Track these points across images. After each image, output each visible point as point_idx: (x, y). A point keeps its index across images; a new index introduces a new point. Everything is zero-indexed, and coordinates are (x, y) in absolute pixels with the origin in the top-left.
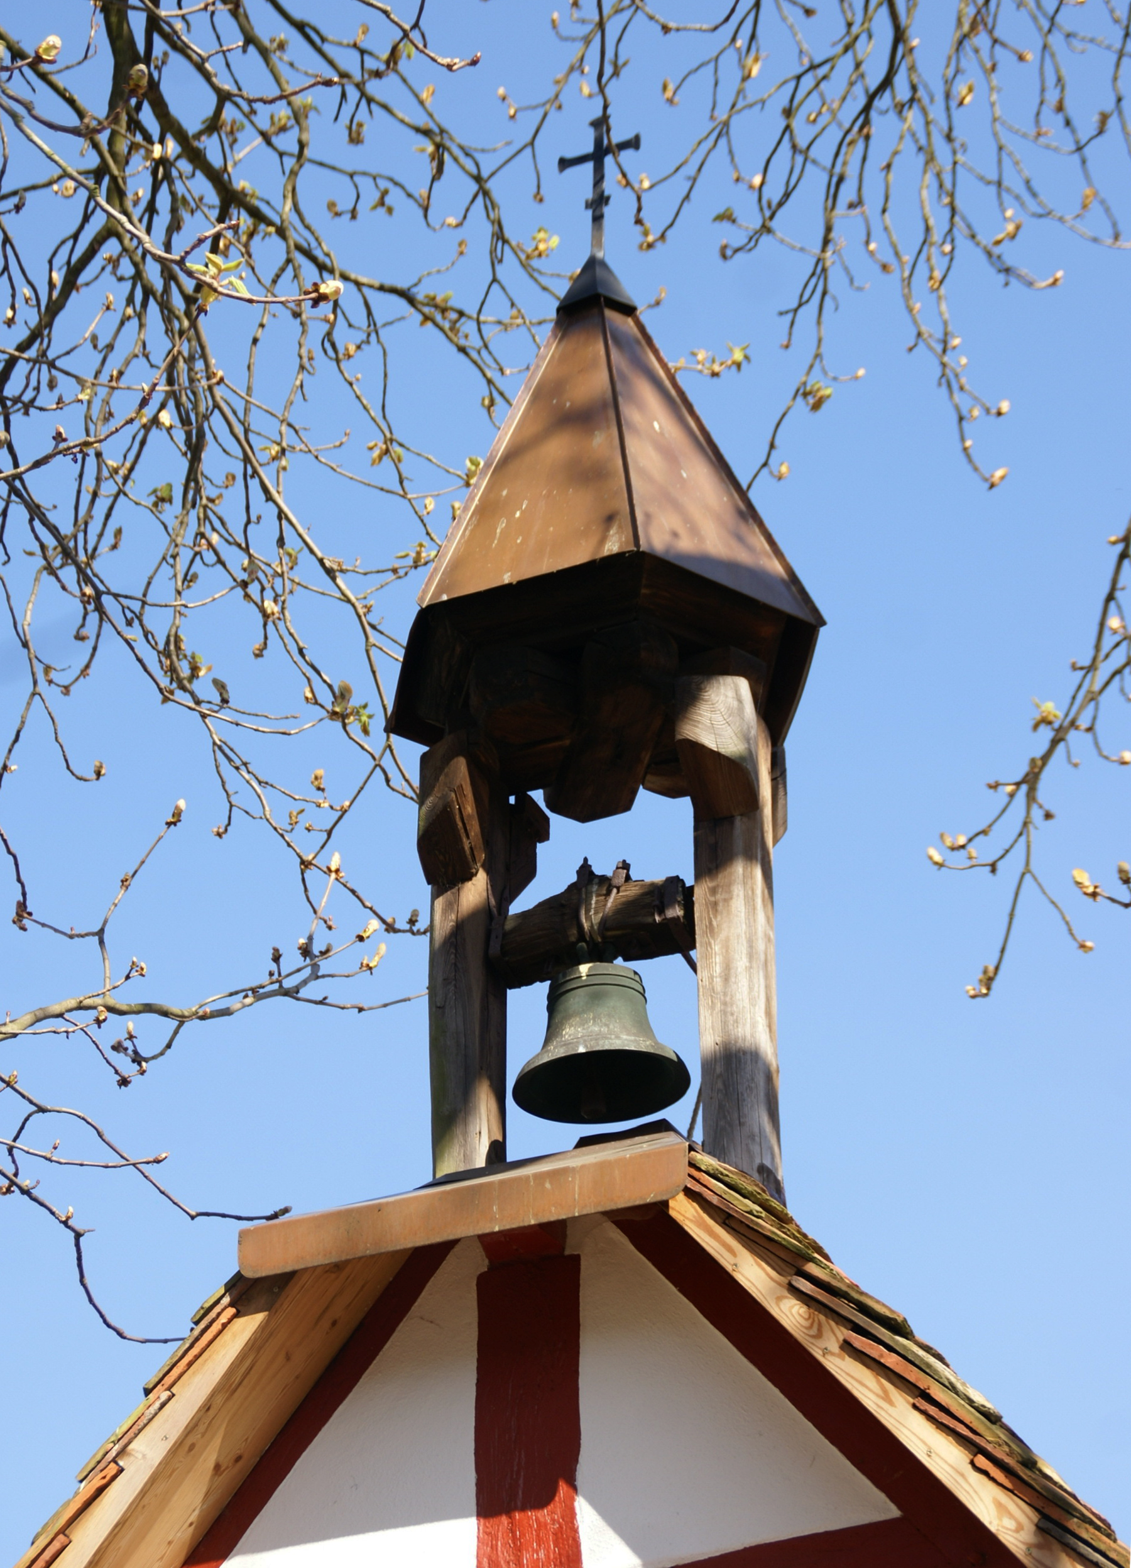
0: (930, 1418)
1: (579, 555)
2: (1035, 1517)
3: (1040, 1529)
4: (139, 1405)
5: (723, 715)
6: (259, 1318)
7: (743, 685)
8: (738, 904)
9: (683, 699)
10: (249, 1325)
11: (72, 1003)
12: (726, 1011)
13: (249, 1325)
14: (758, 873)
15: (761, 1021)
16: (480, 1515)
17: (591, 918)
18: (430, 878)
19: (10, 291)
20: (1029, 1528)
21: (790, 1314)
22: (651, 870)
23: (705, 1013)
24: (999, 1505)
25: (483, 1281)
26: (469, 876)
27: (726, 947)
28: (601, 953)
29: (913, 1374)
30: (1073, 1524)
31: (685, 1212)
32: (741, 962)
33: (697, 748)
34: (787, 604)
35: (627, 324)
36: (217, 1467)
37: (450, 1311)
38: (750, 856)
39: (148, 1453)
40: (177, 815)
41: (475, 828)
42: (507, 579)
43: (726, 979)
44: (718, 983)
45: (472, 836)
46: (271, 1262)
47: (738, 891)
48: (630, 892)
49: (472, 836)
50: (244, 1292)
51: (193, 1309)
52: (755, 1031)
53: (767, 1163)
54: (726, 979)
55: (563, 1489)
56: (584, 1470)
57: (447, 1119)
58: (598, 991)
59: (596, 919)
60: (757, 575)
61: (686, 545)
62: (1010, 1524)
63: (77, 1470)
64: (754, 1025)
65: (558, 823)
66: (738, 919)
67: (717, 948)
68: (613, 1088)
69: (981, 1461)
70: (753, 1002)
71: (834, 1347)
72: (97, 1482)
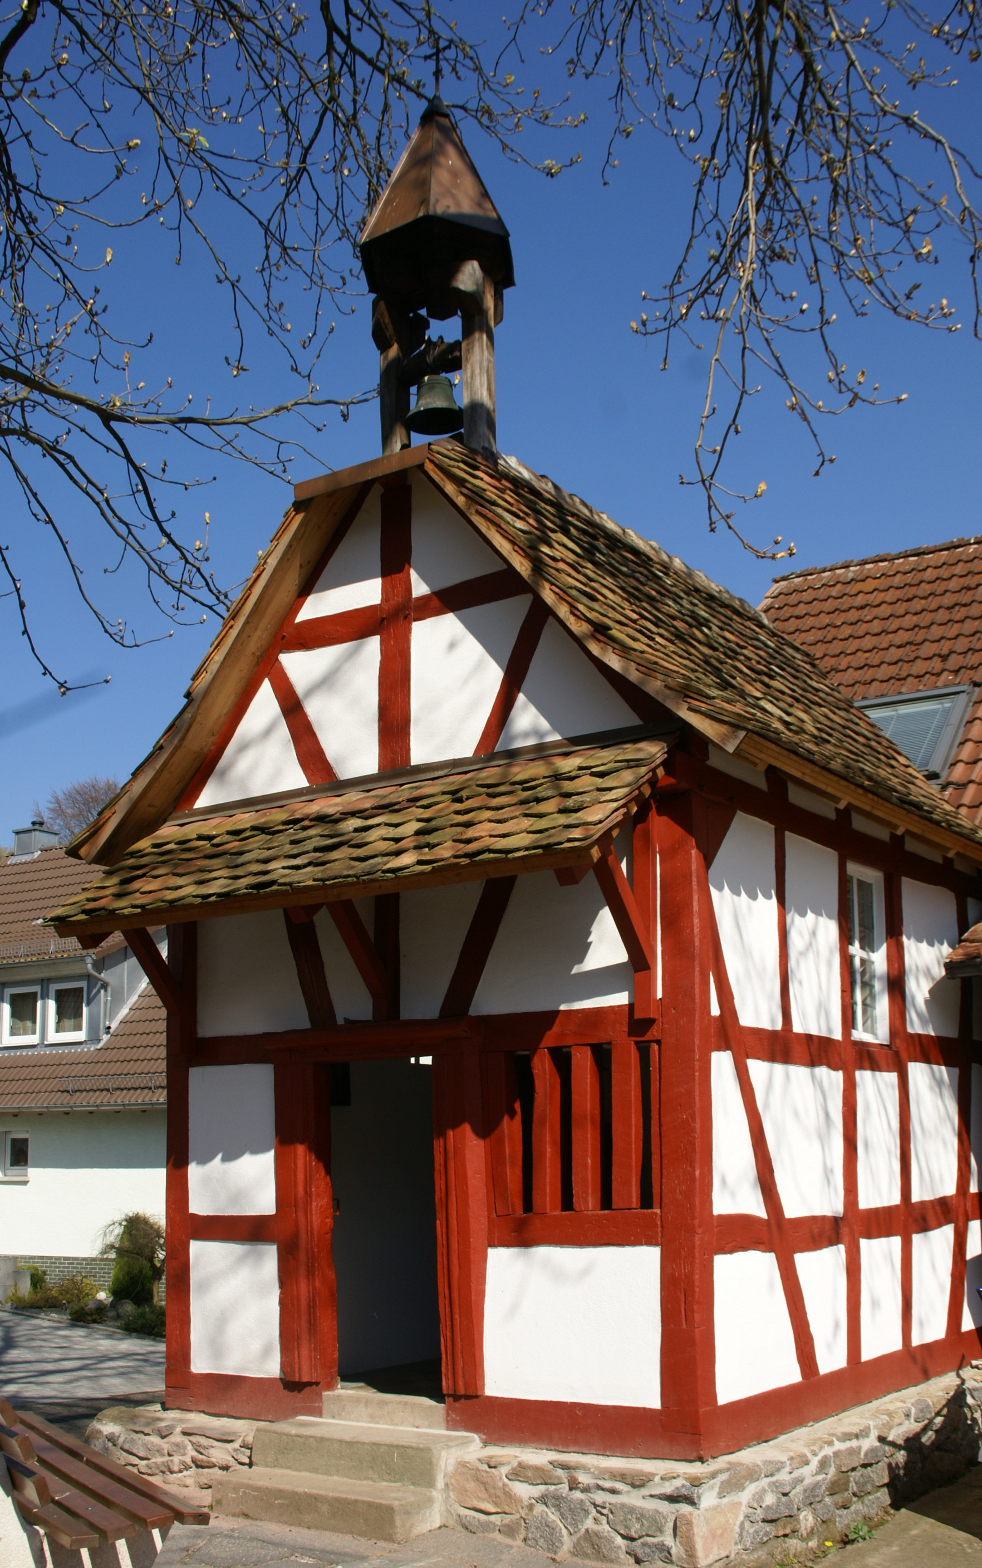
0: (501, 534)
1: (410, 219)
2: (531, 565)
3: (533, 570)
4: (269, 546)
5: (469, 276)
6: (303, 514)
7: (475, 264)
8: (477, 349)
9: (454, 270)
10: (299, 517)
11: (293, 402)
12: (472, 391)
13: (299, 517)
14: (485, 337)
15: (485, 393)
16: (383, 576)
17: (429, 359)
18: (379, 348)
19: (976, 170)
20: (529, 569)
21: (461, 501)
22: (449, 339)
23: (464, 391)
24: (521, 563)
25: (382, 496)
26: (391, 346)
27: (472, 365)
28: (435, 371)
29: (496, 519)
30: (542, 566)
31: (429, 467)
32: (477, 371)
33: (458, 290)
34: (496, 230)
35: (445, 121)
36: (301, 566)
37: (373, 506)
38: (481, 331)
39: (272, 562)
40: (332, 330)
41: (390, 328)
42: (387, 230)
43: (472, 378)
44: (469, 380)
45: (390, 331)
46: (305, 496)
47: (477, 345)
48: (443, 347)
49: (390, 331)
50: (299, 506)
51: (283, 513)
52: (483, 396)
53: (487, 445)
54: (472, 378)
55: (407, 566)
56: (413, 559)
57: (386, 439)
58: (432, 386)
59: (431, 358)
60: (487, 220)
61: (453, 210)
62: (524, 568)
63: (252, 570)
64: (482, 394)
65: (433, 322)
66: (478, 356)
67: (469, 366)
68: (444, 421)
69: (516, 548)
70: (481, 386)
71: (473, 512)
72: (257, 573)
